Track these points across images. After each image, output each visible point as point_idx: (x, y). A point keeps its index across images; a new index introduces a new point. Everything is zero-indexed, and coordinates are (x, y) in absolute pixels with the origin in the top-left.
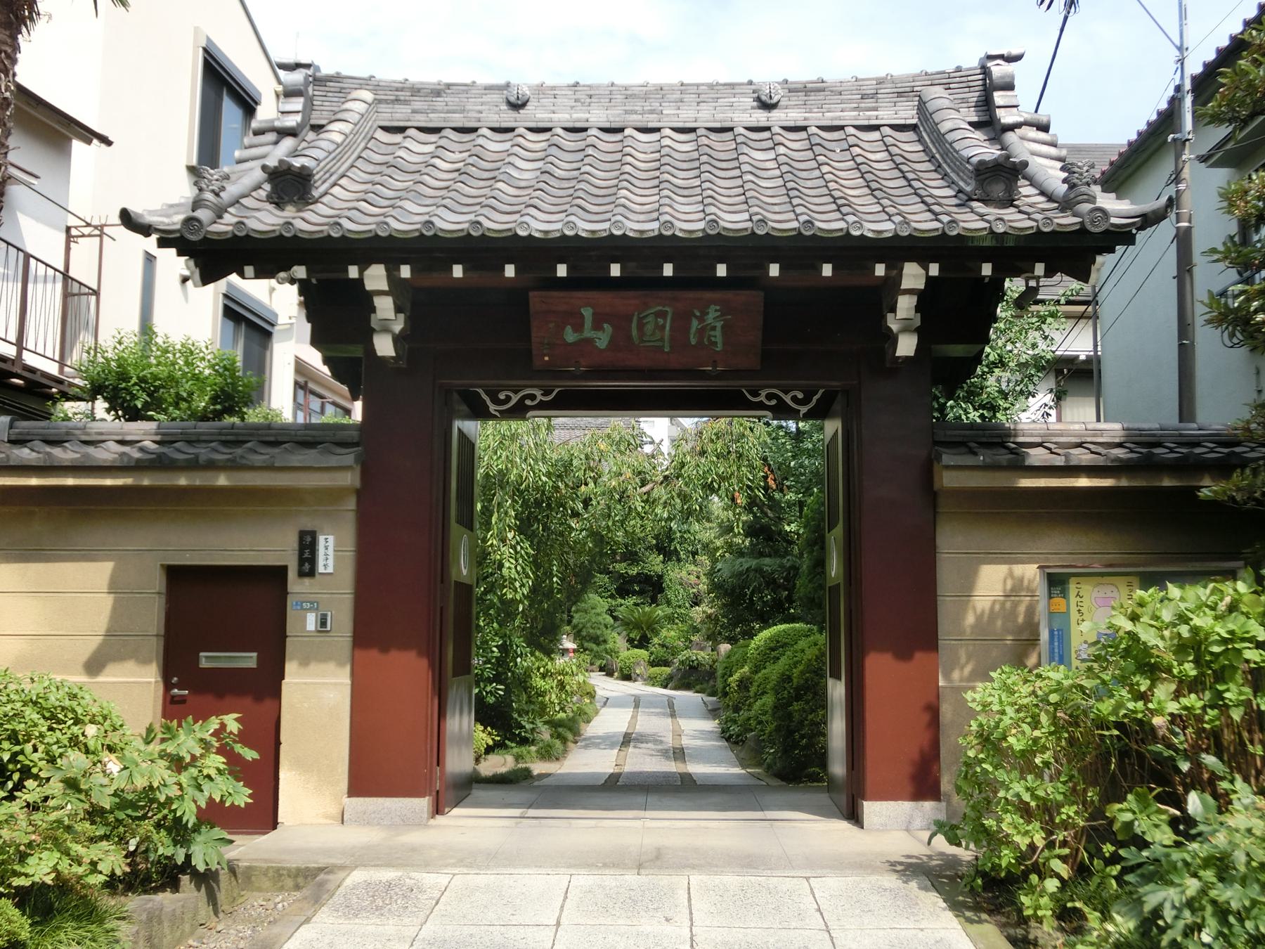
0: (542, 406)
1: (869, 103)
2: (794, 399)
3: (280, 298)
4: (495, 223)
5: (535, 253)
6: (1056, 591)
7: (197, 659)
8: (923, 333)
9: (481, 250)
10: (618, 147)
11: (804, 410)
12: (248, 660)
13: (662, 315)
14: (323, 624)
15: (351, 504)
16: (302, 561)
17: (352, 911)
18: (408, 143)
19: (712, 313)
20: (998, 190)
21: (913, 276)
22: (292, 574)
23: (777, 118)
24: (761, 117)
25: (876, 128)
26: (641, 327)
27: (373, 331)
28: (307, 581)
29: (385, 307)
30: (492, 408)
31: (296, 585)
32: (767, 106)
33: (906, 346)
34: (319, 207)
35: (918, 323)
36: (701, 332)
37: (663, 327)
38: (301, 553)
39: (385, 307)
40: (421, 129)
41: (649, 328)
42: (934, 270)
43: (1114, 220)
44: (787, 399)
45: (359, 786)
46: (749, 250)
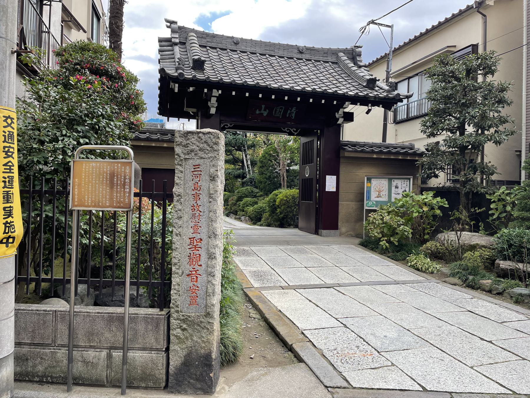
1: (325, 55)
2: (294, 130)
9: (243, 88)
11: (296, 133)
13: (282, 108)
19: (294, 109)
20: (371, 86)
21: (216, 93)
23: (304, 56)
24: (299, 56)
32: (301, 53)
33: (213, 111)
36: (290, 114)
41: (278, 111)
42: (220, 92)
44: (292, 131)
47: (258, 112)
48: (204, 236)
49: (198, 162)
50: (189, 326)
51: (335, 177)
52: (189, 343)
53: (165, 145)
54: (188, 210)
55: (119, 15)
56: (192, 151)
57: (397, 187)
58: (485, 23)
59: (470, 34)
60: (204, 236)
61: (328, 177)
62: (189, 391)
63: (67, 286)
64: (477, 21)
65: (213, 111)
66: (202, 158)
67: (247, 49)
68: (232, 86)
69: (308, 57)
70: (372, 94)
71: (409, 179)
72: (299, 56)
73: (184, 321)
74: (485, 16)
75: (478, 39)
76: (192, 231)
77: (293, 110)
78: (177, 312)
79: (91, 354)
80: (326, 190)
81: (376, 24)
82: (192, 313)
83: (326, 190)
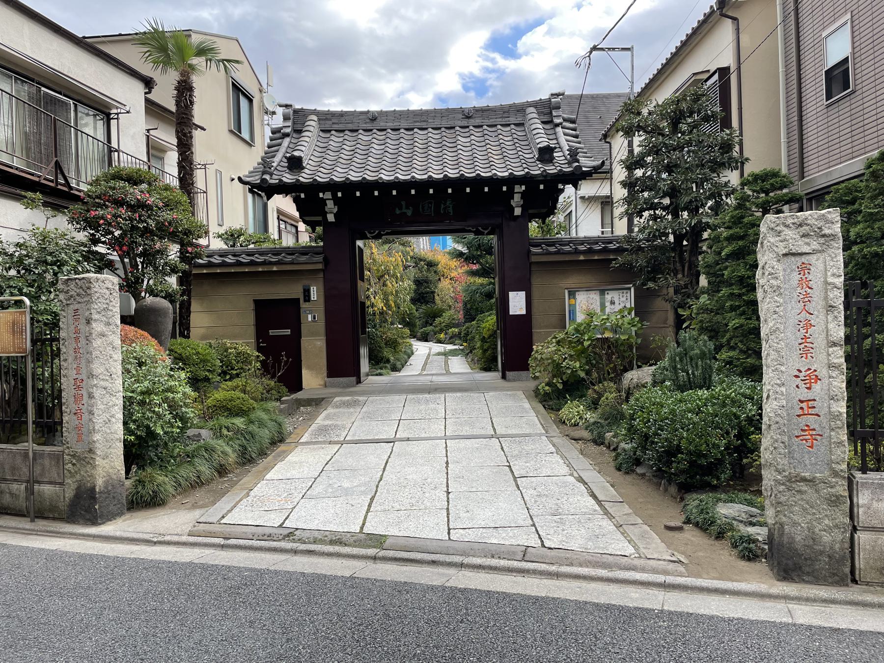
1: (506, 115)
5: (384, 187)
9: (365, 186)
11: (486, 232)
12: (288, 332)
13: (431, 203)
16: (305, 296)
17: (337, 407)
18: (333, 138)
21: (520, 188)
22: (302, 301)
25: (509, 125)
26: (423, 208)
27: (327, 213)
29: (330, 204)
30: (368, 235)
31: (304, 305)
32: (468, 117)
33: (518, 211)
34: (306, 171)
36: (445, 209)
39: (330, 204)
43: (584, 169)
45: (330, 375)
46: (460, 182)
47: (398, 212)
48: (84, 377)
49: (77, 306)
50: (77, 461)
51: (522, 294)
52: (78, 477)
53: (275, 269)
54: (72, 352)
55: (186, 120)
56: (71, 296)
57: (612, 303)
58: (738, 29)
59: (718, 52)
60: (84, 377)
61: (512, 295)
62: (81, 522)
63: (24, 426)
64: (725, 32)
65: (518, 211)
66: (79, 303)
67: (388, 124)
69: (478, 122)
71: (629, 289)
72: (464, 123)
73: (74, 456)
74: (734, 19)
75: (727, 59)
76: (75, 372)
78: (68, 448)
79: (15, 486)
80: (511, 313)
81: (602, 49)
82: (79, 449)
83: (511, 313)
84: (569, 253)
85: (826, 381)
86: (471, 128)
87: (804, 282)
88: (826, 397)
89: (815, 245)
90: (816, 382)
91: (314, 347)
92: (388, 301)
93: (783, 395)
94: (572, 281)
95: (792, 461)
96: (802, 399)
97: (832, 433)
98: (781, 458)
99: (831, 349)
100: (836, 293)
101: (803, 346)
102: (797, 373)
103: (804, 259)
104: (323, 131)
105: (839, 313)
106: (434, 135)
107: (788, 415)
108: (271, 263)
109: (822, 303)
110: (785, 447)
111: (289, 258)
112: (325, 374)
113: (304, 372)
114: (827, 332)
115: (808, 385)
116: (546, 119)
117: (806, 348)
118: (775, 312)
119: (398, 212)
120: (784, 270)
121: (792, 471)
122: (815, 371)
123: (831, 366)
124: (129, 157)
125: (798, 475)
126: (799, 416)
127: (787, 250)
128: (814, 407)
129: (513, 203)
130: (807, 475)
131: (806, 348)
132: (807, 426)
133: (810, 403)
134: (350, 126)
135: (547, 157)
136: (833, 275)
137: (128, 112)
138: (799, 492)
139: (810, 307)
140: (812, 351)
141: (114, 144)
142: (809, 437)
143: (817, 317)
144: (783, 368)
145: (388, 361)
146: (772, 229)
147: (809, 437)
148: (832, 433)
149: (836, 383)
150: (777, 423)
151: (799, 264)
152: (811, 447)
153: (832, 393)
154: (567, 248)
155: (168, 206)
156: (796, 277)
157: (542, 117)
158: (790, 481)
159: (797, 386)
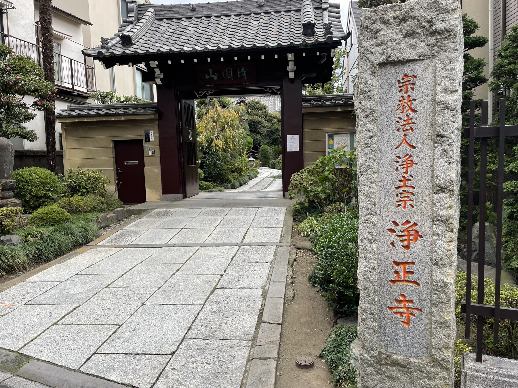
0: (210, 95)
1: (289, 4)
2: (276, 90)
3: (154, 64)
4: (175, 49)
6: (331, 138)
7: (124, 163)
8: (296, 72)
10: (217, 22)
12: (136, 163)
13: (230, 70)
14: (153, 153)
15: (157, 123)
22: (144, 141)
25: (290, 11)
26: (225, 73)
28: (148, 143)
30: (198, 96)
31: (145, 144)
32: (261, 6)
33: (292, 75)
35: (295, 69)
36: (240, 74)
37: (230, 74)
38: (146, 136)
40: (167, 19)
41: (227, 74)
43: (334, 39)
47: (207, 77)
51: (297, 137)
53: (123, 119)
65: (292, 75)
67: (203, 13)
68: (171, 55)
70: (129, 51)
77: (242, 70)
84: (329, 106)
85: (429, 239)
86: (262, 14)
87: (407, 104)
88: (428, 260)
89: (422, 48)
90: (416, 240)
91: (153, 172)
92: (227, 143)
93: (373, 253)
94: (332, 127)
95: (383, 338)
96: (397, 260)
97: (434, 309)
98: (369, 334)
99: (437, 196)
100: (446, 116)
101: (400, 190)
102: (392, 226)
103: (407, 69)
104: (157, 19)
105: (450, 145)
106: (234, 20)
107: (380, 279)
108: (119, 115)
109: (428, 131)
110: (375, 319)
111: (141, 111)
112: (161, 192)
113: (147, 190)
114: (433, 172)
115: (406, 243)
116: (317, 6)
117: (404, 194)
118: (367, 145)
119: (207, 77)
120: (381, 86)
121: (383, 350)
122: (415, 224)
123: (437, 220)
124: (18, 41)
125: (389, 357)
126: (393, 282)
127: (384, 57)
128: (412, 273)
129: (288, 69)
130: (399, 358)
131: (404, 194)
132: (403, 295)
133: (408, 266)
134: (177, 16)
135: (309, 31)
136: (445, 90)
137: (13, 8)
138: (390, 377)
139: (412, 138)
140: (412, 197)
141: (6, 32)
142: (405, 310)
143: (421, 151)
144: (375, 220)
145: (231, 182)
146: (367, 28)
147: (405, 310)
148: (434, 309)
149: (441, 243)
150: (366, 288)
151: (400, 77)
152: (407, 323)
153: (436, 256)
154: (329, 103)
155: (15, 70)
156: (395, 95)
157: (315, 4)
158: (378, 362)
159: (392, 243)
